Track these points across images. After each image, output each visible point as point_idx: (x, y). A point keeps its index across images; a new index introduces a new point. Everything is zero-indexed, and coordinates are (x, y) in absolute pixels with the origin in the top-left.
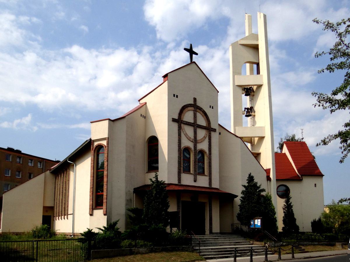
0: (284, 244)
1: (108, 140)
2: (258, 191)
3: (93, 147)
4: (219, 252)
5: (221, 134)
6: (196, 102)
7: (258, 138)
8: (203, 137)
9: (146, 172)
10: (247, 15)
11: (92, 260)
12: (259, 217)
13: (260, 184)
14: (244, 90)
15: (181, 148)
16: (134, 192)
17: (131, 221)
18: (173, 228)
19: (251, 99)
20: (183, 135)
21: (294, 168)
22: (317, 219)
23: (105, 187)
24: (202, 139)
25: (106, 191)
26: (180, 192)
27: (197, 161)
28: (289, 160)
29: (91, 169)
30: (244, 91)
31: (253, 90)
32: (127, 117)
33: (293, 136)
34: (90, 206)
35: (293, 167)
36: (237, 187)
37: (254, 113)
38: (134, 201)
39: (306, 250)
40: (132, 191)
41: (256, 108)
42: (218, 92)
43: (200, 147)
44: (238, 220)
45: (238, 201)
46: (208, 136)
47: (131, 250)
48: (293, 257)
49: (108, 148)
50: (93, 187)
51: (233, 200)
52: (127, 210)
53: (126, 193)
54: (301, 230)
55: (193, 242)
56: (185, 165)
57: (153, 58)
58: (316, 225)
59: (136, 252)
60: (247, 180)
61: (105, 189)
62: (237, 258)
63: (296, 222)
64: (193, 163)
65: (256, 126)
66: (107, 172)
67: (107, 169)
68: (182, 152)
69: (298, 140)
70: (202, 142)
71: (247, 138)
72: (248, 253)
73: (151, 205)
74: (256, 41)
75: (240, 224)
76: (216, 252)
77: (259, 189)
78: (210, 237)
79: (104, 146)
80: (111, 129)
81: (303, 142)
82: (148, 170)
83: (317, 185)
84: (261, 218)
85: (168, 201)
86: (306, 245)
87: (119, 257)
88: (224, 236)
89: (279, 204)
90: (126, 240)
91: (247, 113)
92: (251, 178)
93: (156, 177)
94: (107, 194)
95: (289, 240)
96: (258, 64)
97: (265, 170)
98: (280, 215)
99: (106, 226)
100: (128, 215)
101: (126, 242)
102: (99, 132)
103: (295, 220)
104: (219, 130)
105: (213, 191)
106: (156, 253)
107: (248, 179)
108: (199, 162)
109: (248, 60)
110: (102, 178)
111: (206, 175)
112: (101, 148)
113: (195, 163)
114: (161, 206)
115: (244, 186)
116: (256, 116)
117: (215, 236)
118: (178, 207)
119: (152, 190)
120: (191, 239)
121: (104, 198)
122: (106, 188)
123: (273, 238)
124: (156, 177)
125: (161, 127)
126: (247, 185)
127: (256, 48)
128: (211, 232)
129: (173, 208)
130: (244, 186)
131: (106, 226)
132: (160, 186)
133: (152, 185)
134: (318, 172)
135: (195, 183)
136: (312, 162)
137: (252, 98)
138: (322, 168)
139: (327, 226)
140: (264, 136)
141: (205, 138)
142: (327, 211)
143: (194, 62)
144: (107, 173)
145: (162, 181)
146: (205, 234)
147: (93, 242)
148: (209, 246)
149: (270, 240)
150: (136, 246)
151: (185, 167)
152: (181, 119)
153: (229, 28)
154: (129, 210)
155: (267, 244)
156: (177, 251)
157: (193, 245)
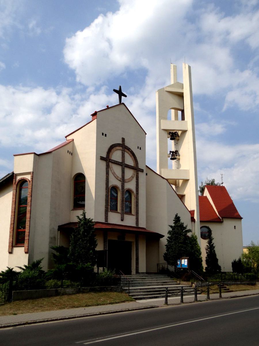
0: (210, 283)
1: (33, 175)
2: (184, 231)
3: (15, 181)
4: (148, 292)
5: (148, 174)
6: (124, 142)
7: (182, 180)
8: (131, 177)
9: (71, 210)
10: (172, 65)
11: (13, 302)
12: (186, 257)
13: (186, 225)
14: (170, 134)
15: (108, 186)
16: (58, 230)
17: (55, 260)
18: (99, 268)
19: (176, 143)
21: (214, 211)
22: (237, 259)
23: (27, 223)
24: (129, 178)
25: (29, 228)
26: (107, 231)
27: (125, 200)
28: (210, 202)
29: (12, 204)
30: (169, 135)
31: (178, 135)
32: (53, 152)
33: (212, 180)
34: (9, 243)
35: (214, 209)
36: (163, 228)
37: (178, 157)
38: (58, 239)
39: (231, 290)
40: (57, 228)
41: (180, 152)
42: (146, 134)
43: (127, 186)
44: (164, 260)
45: (164, 241)
46: (135, 175)
47: (57, 291)
48: (221, 296)
49: (32, 183)
50: (14, 223)
51: (160, 240)
52: (51, 248)
53: (50, 231)
54: (222, 271)
55: (121, 282)
56: (112, 204)
57: (73, 99)
58: (237, 265)
59: (62, 293)
60: (174, 220)
61: (28, 225)
62: (169, 298)
63: (218, 262)
64: (120, 201)
65: (180, 169)
66: (31, 208)
67: (31, 205)
68: (110, 190)
69: (217, 185)
70: (129, 181)
71: (172, 180)
72: (178, 293)
73: (78, 244)
74: (181, 89)
75: (167, 264)
76: (145, 292)
77: (186, 229)
78: (138, 277)
79: (27, 180)
80: (36, 164)
81: (222, 186)
82: (74, 208)
83: (236, 227)
84: (188, 258)
85: (95, 240)
86: (230, 285)
87: (44, 299)
88: (151, 276)
89: (203, 244)
90: (50, 280)
91: (172, 156)
92: (177, 219)
93: (83, 214)
94: (29, 231)
95: (214, 280)
96: (183, 111)
97: (190, 212)
98: (204, 255)
99: (27, 264)
100: (52, 253)
101: (51, 282)
102: (24, 166)
103: (217, 260)
104: (146, 171)
105: (141, 230)
106: (84, 294)
107: (174, 219)
108: (126, 201)
109: (174, 107)
110: (25, 214)
112: (24, 183)
113: (122, 202)
114: (88, 244)
115: (171, 227)
116: (180, 159)
117: (142, 275)
118: (105, 245)
119: (79, 227)
120: (119, 279)
121: (26, 235)
122: (29, 224)
123: (199, 277)
124: (84, 214)
125: (89, 164)
126: (173, 225)
127: (181, 96)
128: (137, 272)
129: (100, 247)
130: (171, 227)
131: (27, 264)
132: (89, 224)
133: (80, 222)
134: (237, 215)
135: (122, 222)
136: (232, 205)
137: (177, 142)
138: (241, 211)
139: (247, 266)
140: (187, 178)
141: (133, 178)
142: (246, 251)
143: (123, 104)
144: (31, 209)
145: (90, 219)
146: (131, 274)
147: (15, 282)
148: (138, 286)
149: (197, 279)
150: (62, 286)
151: (112, 206)
152: (109, 158)
153: (147, 78)
154: (53, 248)
155: (194, 283)
156: (105, 291)
157: (122, 285)
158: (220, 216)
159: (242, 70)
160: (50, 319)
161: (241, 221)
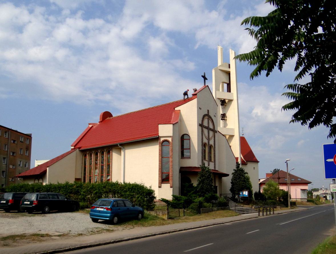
20: (203, 135)
31: (226, 102)
41: (227, 115)
57: (47, 20)
65: (227, 127)
83: (255, 168)
84: (248, 190)
111: (213, 161)
127: (229, 74)
140: (233, 135)
158: (245, 160)
159: (210, 11)
160: (217, 223)
161: (258, 164)
